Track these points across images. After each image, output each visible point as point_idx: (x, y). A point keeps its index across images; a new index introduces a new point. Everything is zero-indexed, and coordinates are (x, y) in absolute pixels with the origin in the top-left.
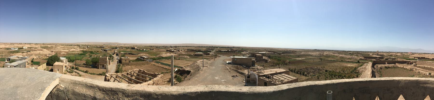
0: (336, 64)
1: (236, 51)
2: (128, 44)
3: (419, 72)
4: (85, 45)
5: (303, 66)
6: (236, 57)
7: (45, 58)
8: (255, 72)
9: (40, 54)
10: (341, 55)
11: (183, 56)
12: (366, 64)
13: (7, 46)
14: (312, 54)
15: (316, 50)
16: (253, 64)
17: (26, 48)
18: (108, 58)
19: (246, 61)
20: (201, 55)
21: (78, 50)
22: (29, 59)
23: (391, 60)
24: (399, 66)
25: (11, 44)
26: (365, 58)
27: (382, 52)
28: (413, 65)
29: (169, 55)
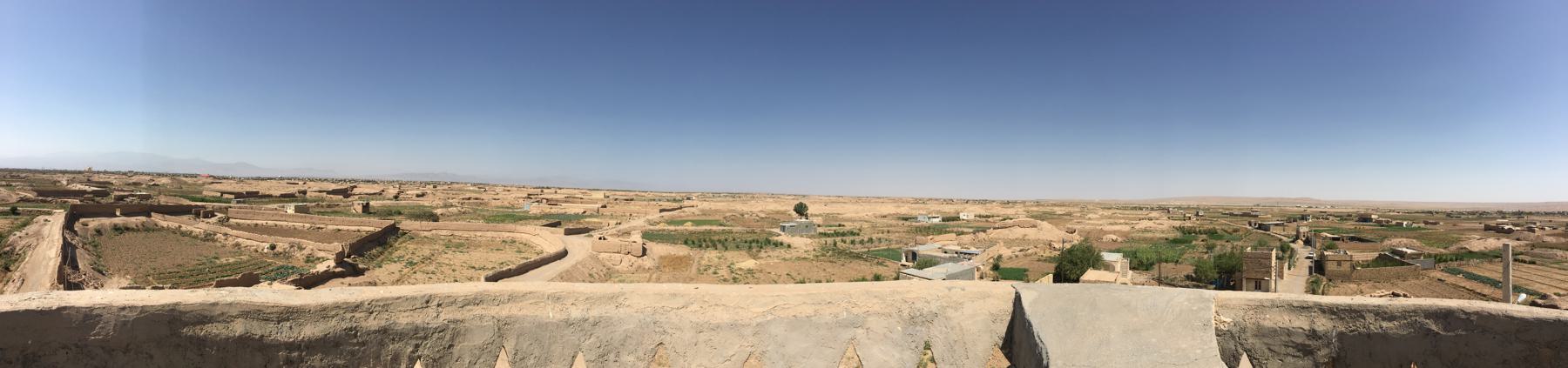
2: (1346, 205)
3: (238, 245)
4: (1188, 208)
7: (1047, 254)
9: (1024, 240)
11: (1550, 252)
12: (41, 218)
13: (904, 210)
17: (972, 217)
18: (1274, 253)
21: (1163, 226)
22: (984, 256)
23: (136, 201)
24: (164, 224)
25: (917, 201)
26: (40, 193)
27: (105, 172)
28: (213, 220)
29: (1493, 243)
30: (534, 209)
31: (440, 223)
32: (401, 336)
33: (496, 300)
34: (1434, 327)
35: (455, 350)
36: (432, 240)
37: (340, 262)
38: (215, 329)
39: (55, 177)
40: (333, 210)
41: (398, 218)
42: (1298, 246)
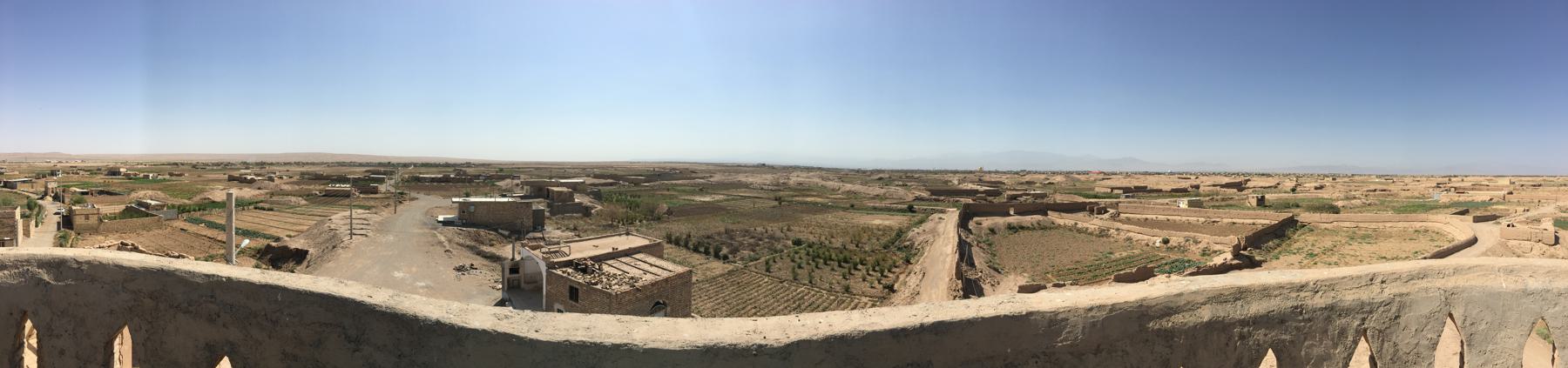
0: (830, 218)
1: (478, 177)
2: (96, 158)
3: (1129, 239)
5: (716, 226)
6: (472, 199)
8: (537, 252)
10: (848, 187)
12: (936, 216)
14: (750, 180)
15: (762, 168)
16: (538, 222)
18: (18, 212)
19: (506, 212)
20: (347, 195)
23: (1030, 200)
24: (1061, 222)
26: (933, 193)
28: (1106, 216)
30: (1443, 198)
31: (1342, 215)
32: (1347, 312)
33: (1440, 273)
34: (46, 277)
35: (1402, 320)
36: (1335, 232)
37: (1236, 255)
38: (1178, 319)
39: (947, 177)
40: (1226, 203)
41: (1297, 211)
42: (48, 203)
